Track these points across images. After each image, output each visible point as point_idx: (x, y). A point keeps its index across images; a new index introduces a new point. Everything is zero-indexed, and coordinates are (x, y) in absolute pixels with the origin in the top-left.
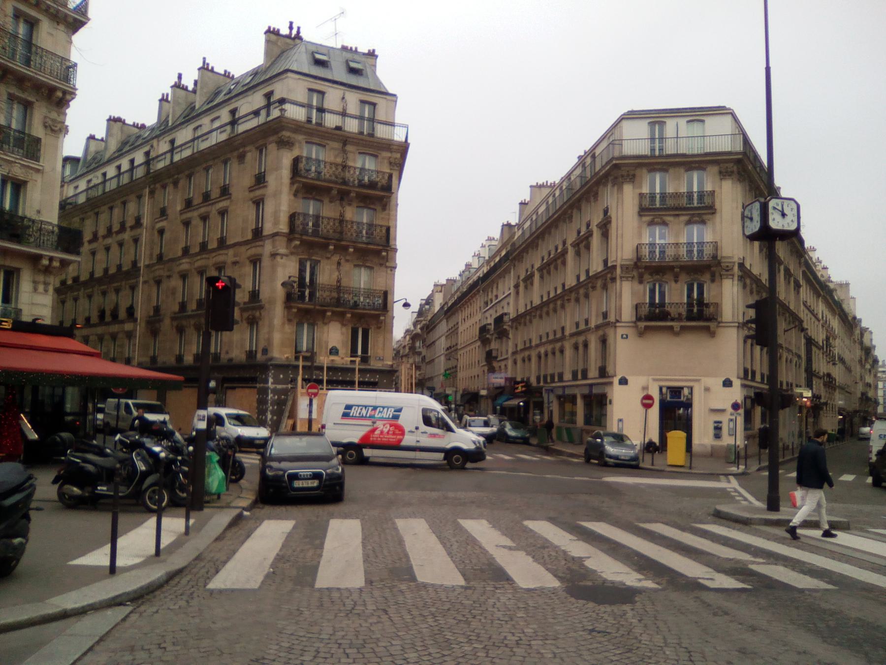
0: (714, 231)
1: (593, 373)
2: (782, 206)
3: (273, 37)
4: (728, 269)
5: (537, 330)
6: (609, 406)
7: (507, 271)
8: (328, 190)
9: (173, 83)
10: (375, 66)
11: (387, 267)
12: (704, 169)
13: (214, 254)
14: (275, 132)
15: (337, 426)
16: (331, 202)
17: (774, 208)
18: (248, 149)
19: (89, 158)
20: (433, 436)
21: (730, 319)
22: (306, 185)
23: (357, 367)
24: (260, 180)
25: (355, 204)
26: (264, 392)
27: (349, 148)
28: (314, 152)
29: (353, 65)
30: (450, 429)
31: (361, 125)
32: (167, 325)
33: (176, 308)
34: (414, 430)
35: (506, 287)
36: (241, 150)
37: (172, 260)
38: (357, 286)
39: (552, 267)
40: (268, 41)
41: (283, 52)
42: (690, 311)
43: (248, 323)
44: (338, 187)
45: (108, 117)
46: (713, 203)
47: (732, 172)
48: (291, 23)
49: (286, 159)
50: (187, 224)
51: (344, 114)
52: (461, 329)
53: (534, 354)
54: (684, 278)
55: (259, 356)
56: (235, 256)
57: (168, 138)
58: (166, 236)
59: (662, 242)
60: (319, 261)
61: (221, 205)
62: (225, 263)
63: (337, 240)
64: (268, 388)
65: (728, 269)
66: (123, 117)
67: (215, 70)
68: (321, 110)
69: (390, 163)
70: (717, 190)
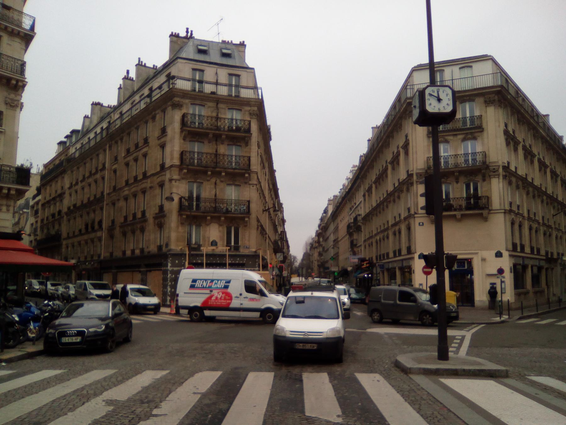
0: (483, 144)
1: (404, 251)
2: (438, 92)
3: (175, 39)
4: (495, 171)
5: (377, 223)
6: (413, 274)
7: (359, 186)
8: (205, 135)
9: (123, 77)
10: (244, 52)
11: (250, 184)
12: (473, 101)
13: (140, 183)
14: (172, 99)
15: (187, 295)
16: (209, 142)
17: (431, 95)
18: (157, 112)
19: (85, 130)
20: (252, 300)
21: (498, 208)
22: (191, 133)
23: (227, 253)
24: (164, 131)
25: (226, 143)
26: (165, 272)
27: (221, 105)
28: (197, 110)
29: (225, 51)
30: (263, 294)
31: (230, 90)
32: (117, 231)
33: (122, 220)
34: (239, 296)
35: (359, 198)
36: (154, 113)
37: (120, 189)
38: (230, 198)
39: (381, 180)
40: (171, 42)
41: (181, 48)
42: (468, 203)
43: (159, 227)
44: (226, 133)
45: (91, 103)
46: (481, 124)
47: (494, 101)
48: (187, 29)
49: (177, 116)
50: (127, 164)
51: (217, 84)
52: (340, 228)
53: (374, 240)
54: (462, 179)
55: (164, 248)
56: (151, 183)
57: (119, 112)
58: (118, 173)
59: (446, 154)
60: (202, 183)
61: (145, 150)
62: (146, 188)
63: (213, 168)
64: (167, 270)
65: (495, 171)
66: (101, 102)
67: (147, 65)
68: (201, 82)
69: (250, 114)
70: (483, 114)
